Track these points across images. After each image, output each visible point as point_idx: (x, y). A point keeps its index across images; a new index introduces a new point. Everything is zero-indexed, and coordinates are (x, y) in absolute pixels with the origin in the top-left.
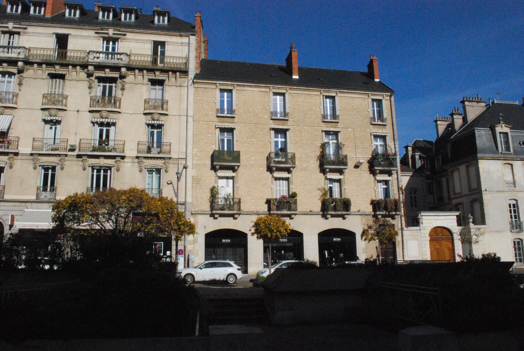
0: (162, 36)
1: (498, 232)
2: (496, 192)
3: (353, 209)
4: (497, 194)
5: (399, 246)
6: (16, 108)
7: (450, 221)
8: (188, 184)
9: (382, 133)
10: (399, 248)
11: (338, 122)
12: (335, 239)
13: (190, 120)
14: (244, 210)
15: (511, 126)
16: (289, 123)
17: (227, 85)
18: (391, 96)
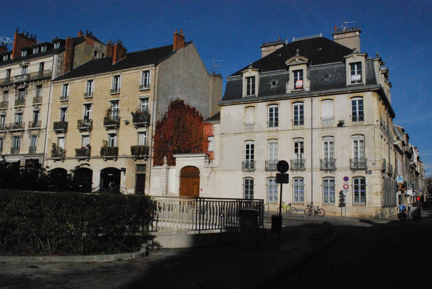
0: (42, 59)
1: (229, 170)
2: (233, 135)
3: (120, 153)
4: (234, 136)
5: (147, 180)
6: (25, 107)
7: (199, 161)
9: (146, 96)
10: (147, 181)
11: (68, 101)
12: (109, 175)
13: (50, 105)
14: (67, 157)
16: (94, 99)
18: (156, 66)
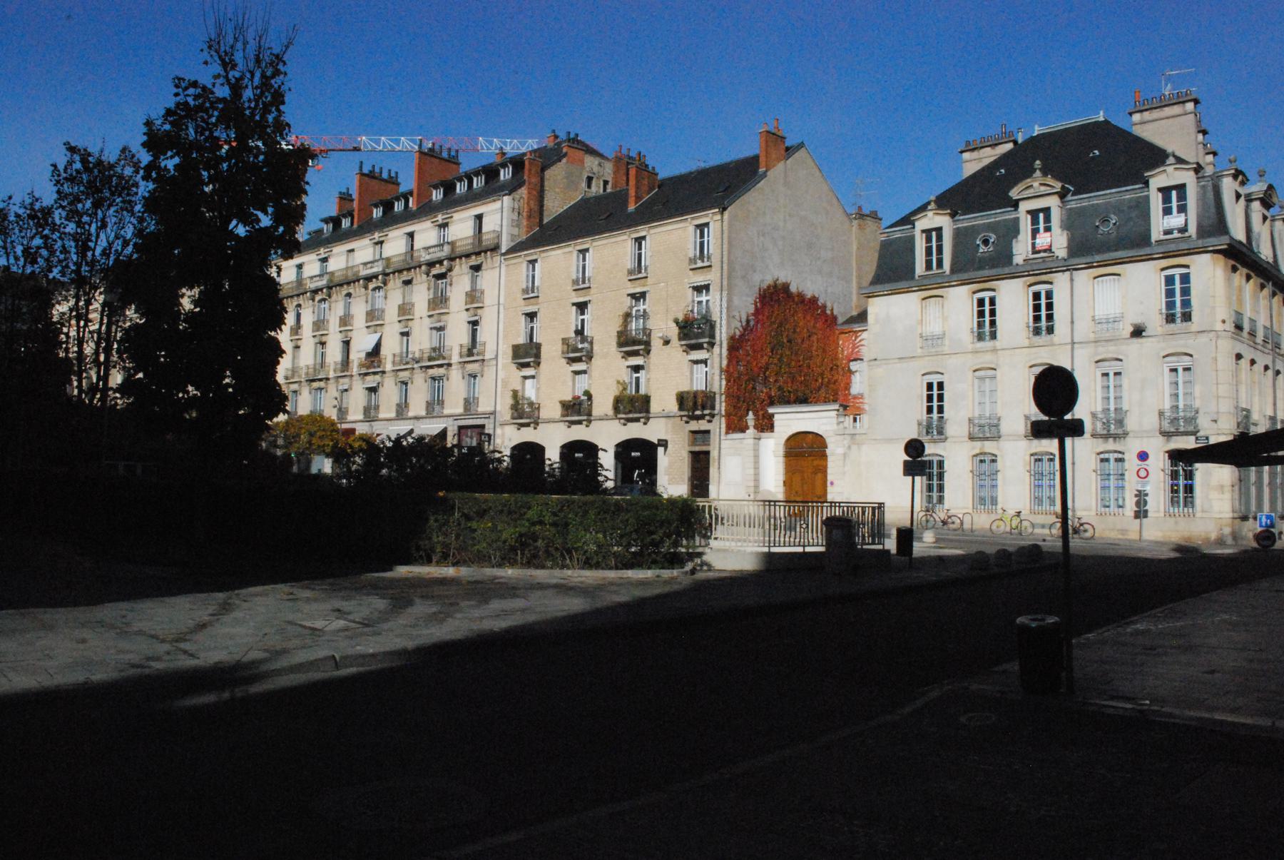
2: (897, 361)
7: (825, 421)
8: (915, 500)
13: (501, 307)
15: (949, 211)
16: (592, 291)
17: (531, 254)
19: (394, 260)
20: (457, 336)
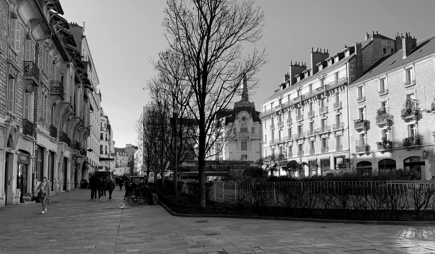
13: (349, 107)
19: (286, 104)
20: (331, 121)
